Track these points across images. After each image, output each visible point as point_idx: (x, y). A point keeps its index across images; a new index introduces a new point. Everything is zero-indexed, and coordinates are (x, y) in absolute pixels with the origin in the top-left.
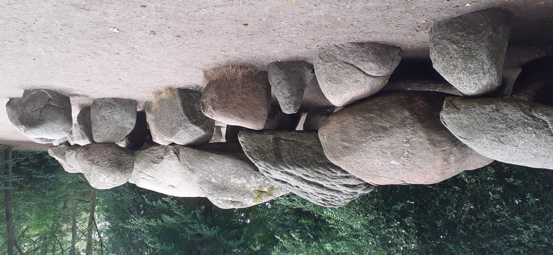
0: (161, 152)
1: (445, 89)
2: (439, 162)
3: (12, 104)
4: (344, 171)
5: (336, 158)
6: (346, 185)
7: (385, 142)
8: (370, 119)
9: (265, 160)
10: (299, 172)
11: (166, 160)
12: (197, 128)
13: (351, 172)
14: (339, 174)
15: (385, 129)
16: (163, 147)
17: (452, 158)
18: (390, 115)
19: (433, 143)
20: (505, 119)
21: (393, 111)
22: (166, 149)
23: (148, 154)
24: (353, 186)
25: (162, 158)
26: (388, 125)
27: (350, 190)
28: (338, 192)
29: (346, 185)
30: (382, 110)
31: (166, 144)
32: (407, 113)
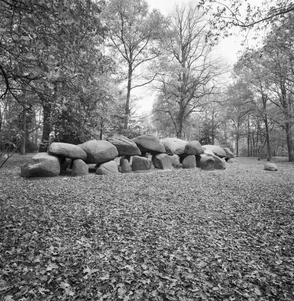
0: (177, 152)
1: (51, 161)
2: (88, 146)
3: (89, 169)
4: (112, 144)
5: (113, 147)
6: (113, 140)
7: (101, 151)
8: (104, 156)
9: (133, 147)
10: (125, 144)
11: (175, 151)
12: (158, 158)
13: (111, 144)
14: (114, 143)
15: (101, 154)
16: (176, 154)
17: (85, 146)
18: (98, 157)
19: (89, 150)
20: (74, 153)
21: (98, 158)
22: (175, 153)
23: (182, 152)
24: (111, 140)
25: (176, 150)
26: (100, 155)
27: (112, 139)
28: (115, 138)
29: (113, 140)
30: (101, 159)
31: (175, 155)
32: (95, 157)
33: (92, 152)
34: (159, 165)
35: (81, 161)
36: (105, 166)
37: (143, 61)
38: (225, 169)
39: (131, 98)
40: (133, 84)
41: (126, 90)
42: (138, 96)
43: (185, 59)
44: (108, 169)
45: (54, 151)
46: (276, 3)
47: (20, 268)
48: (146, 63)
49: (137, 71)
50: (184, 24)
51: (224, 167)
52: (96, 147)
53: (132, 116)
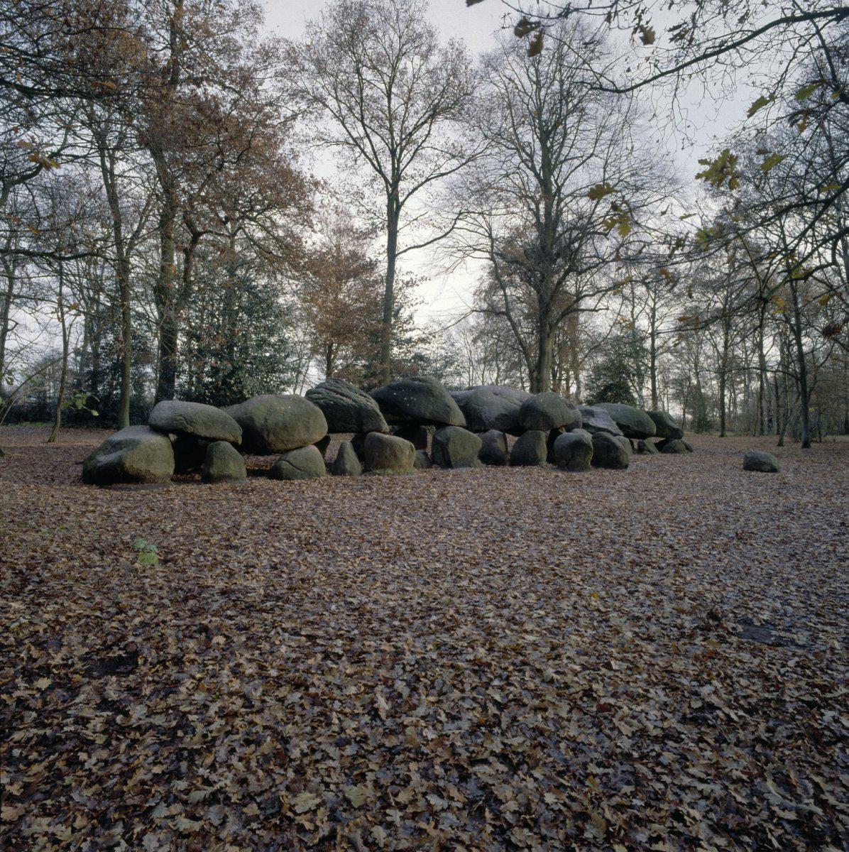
1: (447, 406)
2: (250, 408)
19: (251, 419)
33: (259, 422)
34: (441, 459)
35: (228, 444)
36: (291, 460)
37: (428, 180)
38: (626, 467)
39: (401, 277)
40: (402, 240)
41: (384, 258)
42: (418, 273)
43: (548, 167)
44: (298, 465)
45: (159, 423)
46: (766, 11)
47: (489, 659)
48: (438, 185)
49: (412, 206)
50: (76, 153)
51: (625, 462)
52: (270, 411)
53: (406, 327)
